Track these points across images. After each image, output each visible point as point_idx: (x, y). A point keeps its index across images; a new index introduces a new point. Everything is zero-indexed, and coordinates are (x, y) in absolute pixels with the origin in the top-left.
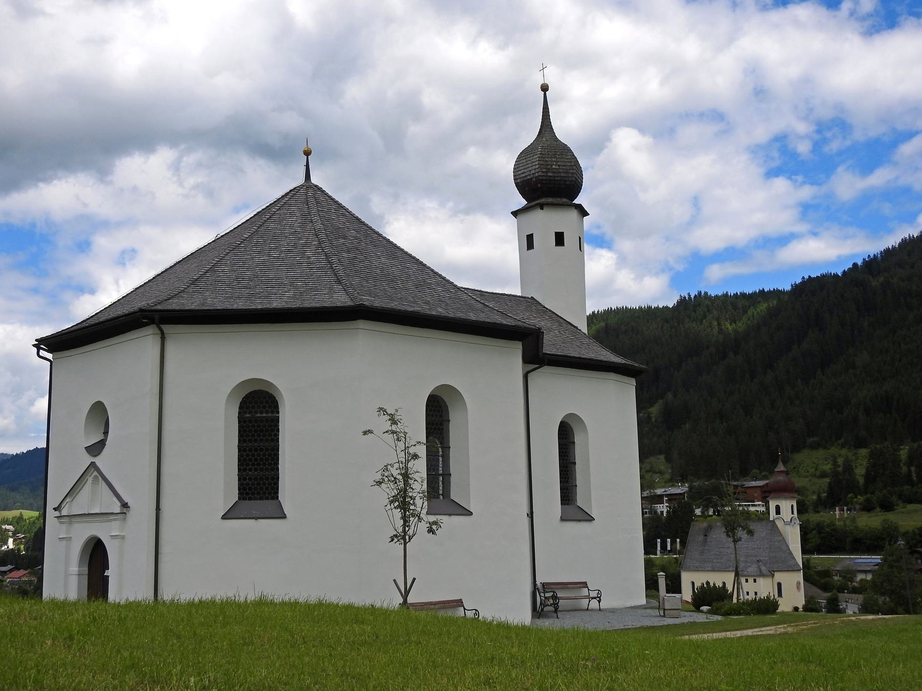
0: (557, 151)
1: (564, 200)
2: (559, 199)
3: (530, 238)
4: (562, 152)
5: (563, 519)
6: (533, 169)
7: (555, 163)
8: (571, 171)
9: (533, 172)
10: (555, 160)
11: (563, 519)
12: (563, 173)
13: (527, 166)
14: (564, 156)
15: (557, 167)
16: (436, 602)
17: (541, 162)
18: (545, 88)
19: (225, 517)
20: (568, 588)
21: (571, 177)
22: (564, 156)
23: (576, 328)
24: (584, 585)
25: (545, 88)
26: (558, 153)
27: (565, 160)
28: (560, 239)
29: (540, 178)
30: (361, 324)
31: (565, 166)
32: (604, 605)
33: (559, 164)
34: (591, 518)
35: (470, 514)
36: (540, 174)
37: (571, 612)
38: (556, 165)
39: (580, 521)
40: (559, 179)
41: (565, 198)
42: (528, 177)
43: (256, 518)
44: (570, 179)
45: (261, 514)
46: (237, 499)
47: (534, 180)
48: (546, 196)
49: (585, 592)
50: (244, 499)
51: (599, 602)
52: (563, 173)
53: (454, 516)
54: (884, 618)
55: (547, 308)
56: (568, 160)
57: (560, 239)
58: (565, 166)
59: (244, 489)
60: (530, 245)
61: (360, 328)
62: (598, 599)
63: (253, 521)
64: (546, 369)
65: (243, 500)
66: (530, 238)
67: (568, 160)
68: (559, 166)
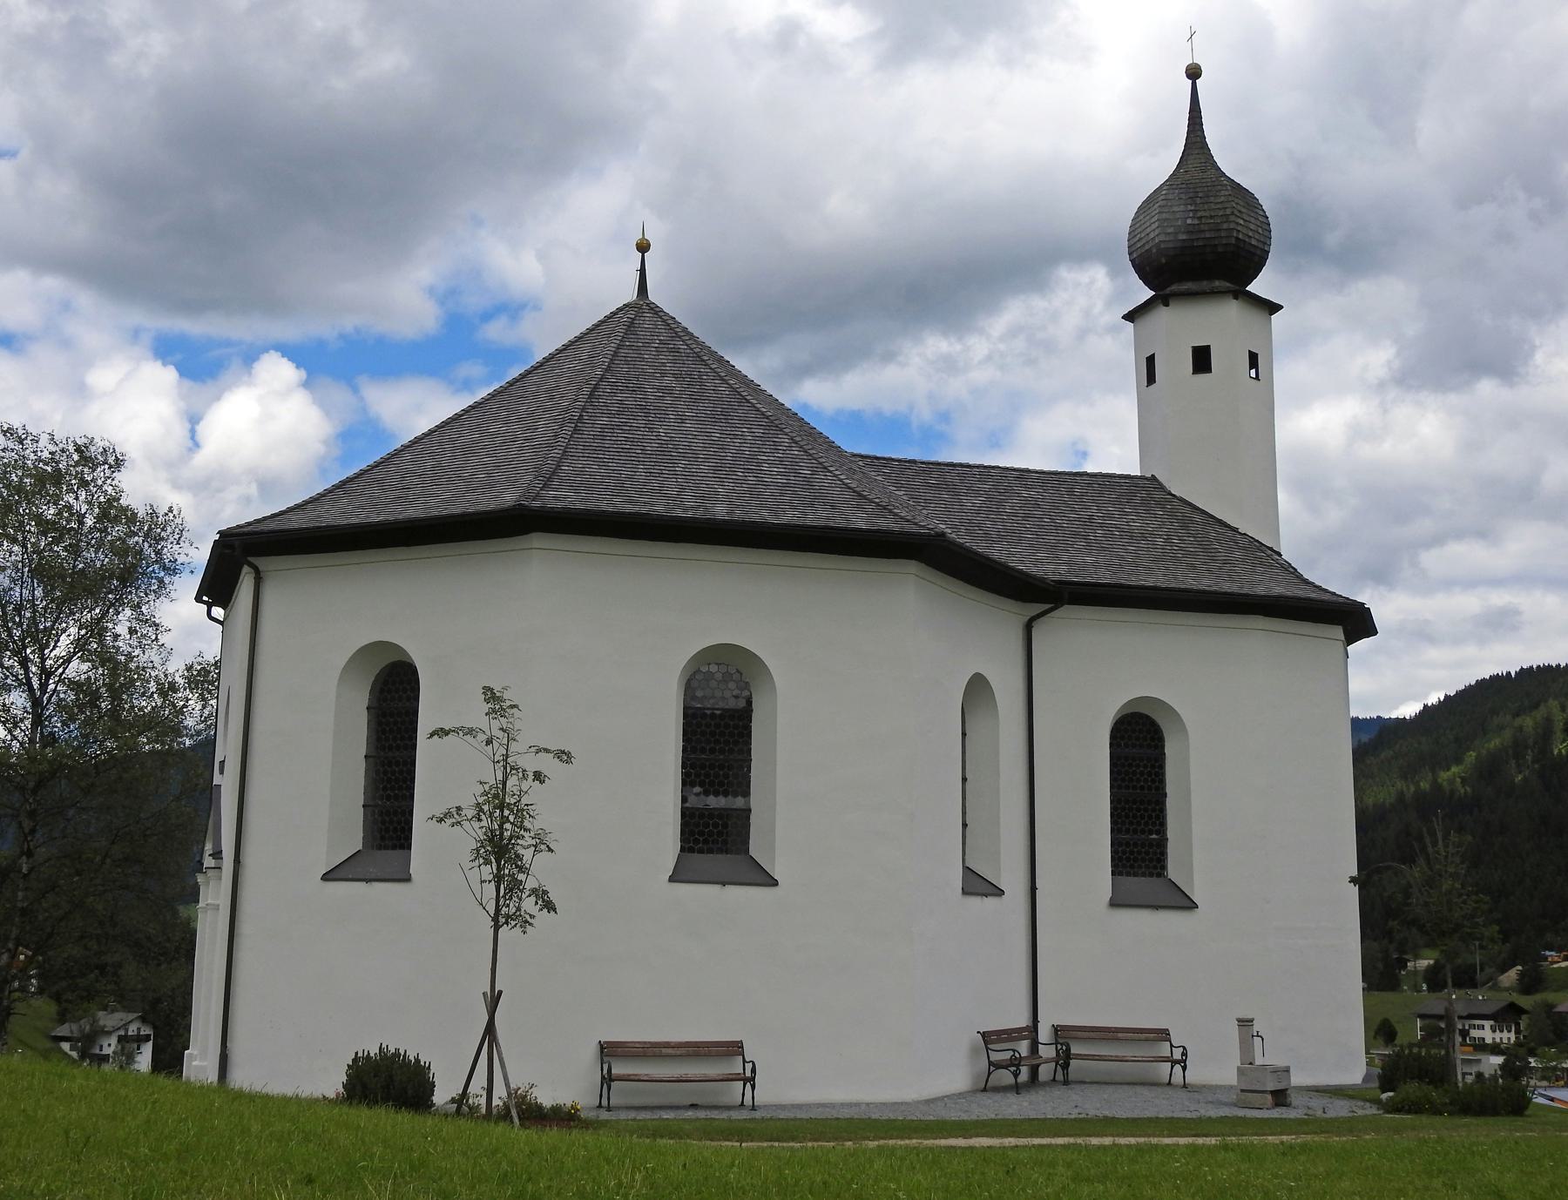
0: (1198, 190)
1: (1217, 283)
2: (1205, 283)
3: (1151, 361)
4: (1208, 191)
5: (1114, 904)
6: (1155, 234)
7: (1191, 215)
8: (1225, 226)
9: (1152, 236)
10: (1193, 208)
11: (1114, 904)
12: (1210, 230)
13: (1143, 227)
14: (1212, 199)
15: (1196, 222)
16: (680, 1043)
17: (1164, 216)
18: (1194, 73)
19: (327, 877)
20: (1118, 1039)
21: (1227, 237)
22: (1212, 199)
23: (1235, 530)
24: (1163, 1035)
25: (1194, 73)
26: (1200, 195)
27: (1213, 206)
28: (1202, 360)
29: (1162, 246)
30: (537, 540)
31: (1211, 217)
32: (1193, 1076)
33: (1199, 214)
34: (1189, 904)
35: (775, 883)
36: (1162, 238)
37: (1139, 1089)
38: (1193, 218)
39: (1157, 907)
40: (1201, 243)
41: (1218, 279)
42: (1147, 247)
43: (368, 881)
44: (1224, 242)
45: (379, 874)
46: (360, 847)
47: (1154, 251)
48: (1181, 280)
49: (1164, 1050)
50: (691, 850)
51: (1184, 1069)
52: (1210, 230)
53: (732, 887)
54: (971, 1148)
55: (1174, 495)
56: (1218, 206)
57: (1202, 360)
58: (1211, 217)
59: (692, 833)
60: (1151, 379)
61: (533, 547)
62: (1013, 1069)
63: (717, 888)
64: (1067, 612)
65: (689, 852)
66: (1151, 361)
67: (1218, 206)
68: (1200, 218)
